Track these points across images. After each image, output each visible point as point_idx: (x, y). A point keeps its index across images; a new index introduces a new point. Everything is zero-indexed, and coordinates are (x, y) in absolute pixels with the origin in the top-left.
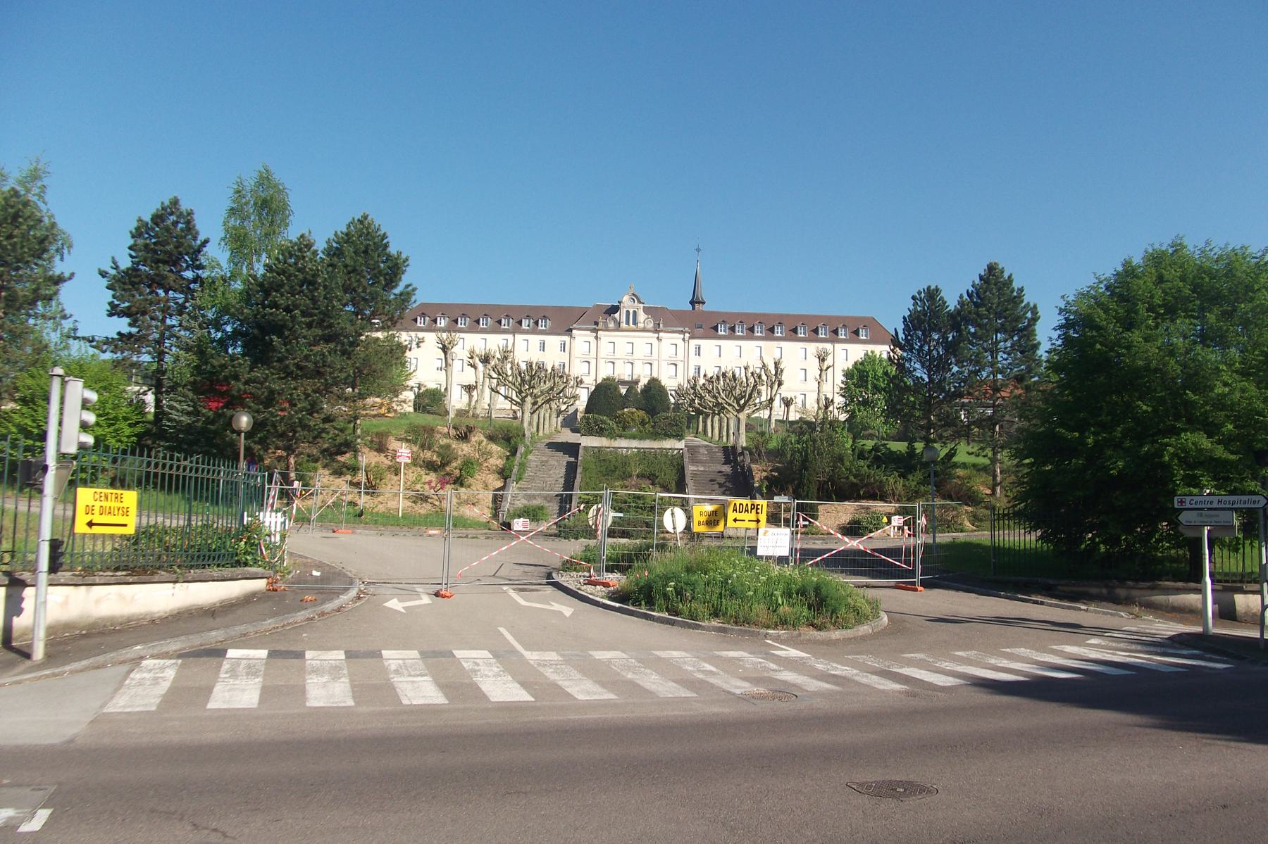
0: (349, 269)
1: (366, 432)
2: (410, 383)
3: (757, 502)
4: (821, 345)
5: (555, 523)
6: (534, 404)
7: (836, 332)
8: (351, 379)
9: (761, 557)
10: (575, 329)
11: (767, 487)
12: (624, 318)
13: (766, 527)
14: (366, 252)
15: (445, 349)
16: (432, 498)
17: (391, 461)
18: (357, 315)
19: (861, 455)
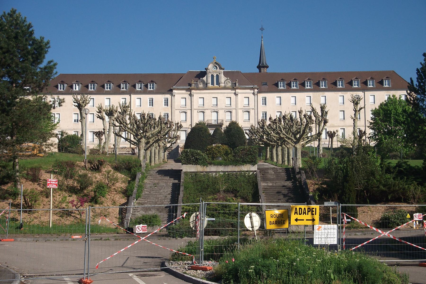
0: (4, 50)
1: (23, 168)
2: (56, 132)
3: (312, 206)
4: (355, 93)
5: (166, 227)
6: (147, 143)
7: (365, 83)
8: (10, 130)
9: (317, 246)
10: (175, 89)
11: (318, 196)
12: (210, 81)
13: (320, 224)
14: (16, 37)
15: (80, 107)
16: (75, 213)
17: (43, 188)
18: (12, 84)
19: (388, 170)
